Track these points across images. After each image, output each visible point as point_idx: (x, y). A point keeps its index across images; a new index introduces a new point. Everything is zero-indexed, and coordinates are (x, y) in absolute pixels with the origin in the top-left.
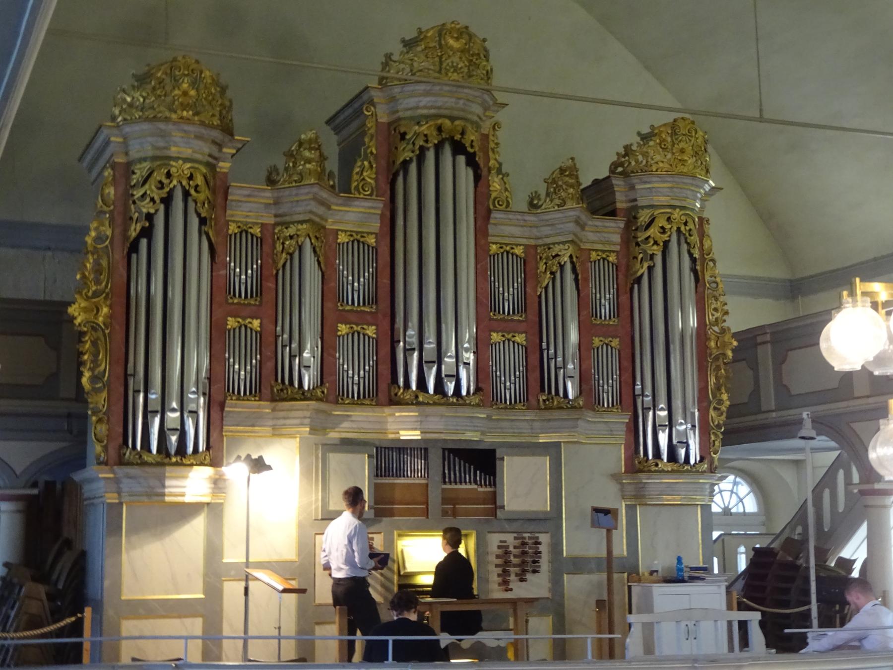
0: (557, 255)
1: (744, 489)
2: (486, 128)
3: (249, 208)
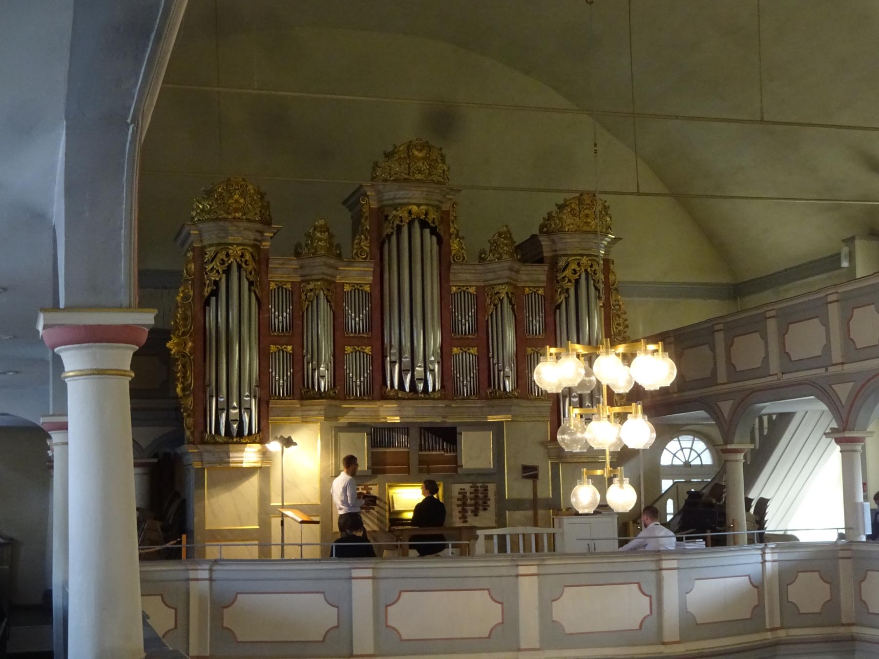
0: (498, 293)
1: (700, 445)
2: (446, 207)
3: (283, 272)
